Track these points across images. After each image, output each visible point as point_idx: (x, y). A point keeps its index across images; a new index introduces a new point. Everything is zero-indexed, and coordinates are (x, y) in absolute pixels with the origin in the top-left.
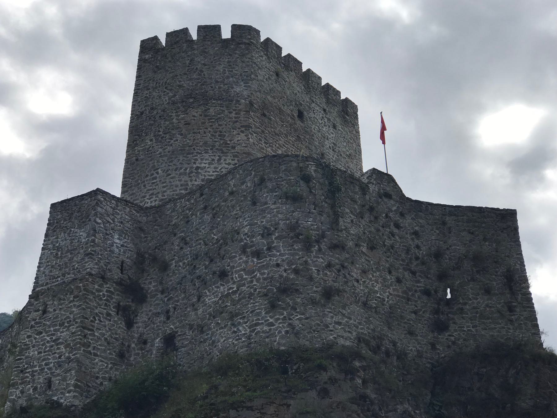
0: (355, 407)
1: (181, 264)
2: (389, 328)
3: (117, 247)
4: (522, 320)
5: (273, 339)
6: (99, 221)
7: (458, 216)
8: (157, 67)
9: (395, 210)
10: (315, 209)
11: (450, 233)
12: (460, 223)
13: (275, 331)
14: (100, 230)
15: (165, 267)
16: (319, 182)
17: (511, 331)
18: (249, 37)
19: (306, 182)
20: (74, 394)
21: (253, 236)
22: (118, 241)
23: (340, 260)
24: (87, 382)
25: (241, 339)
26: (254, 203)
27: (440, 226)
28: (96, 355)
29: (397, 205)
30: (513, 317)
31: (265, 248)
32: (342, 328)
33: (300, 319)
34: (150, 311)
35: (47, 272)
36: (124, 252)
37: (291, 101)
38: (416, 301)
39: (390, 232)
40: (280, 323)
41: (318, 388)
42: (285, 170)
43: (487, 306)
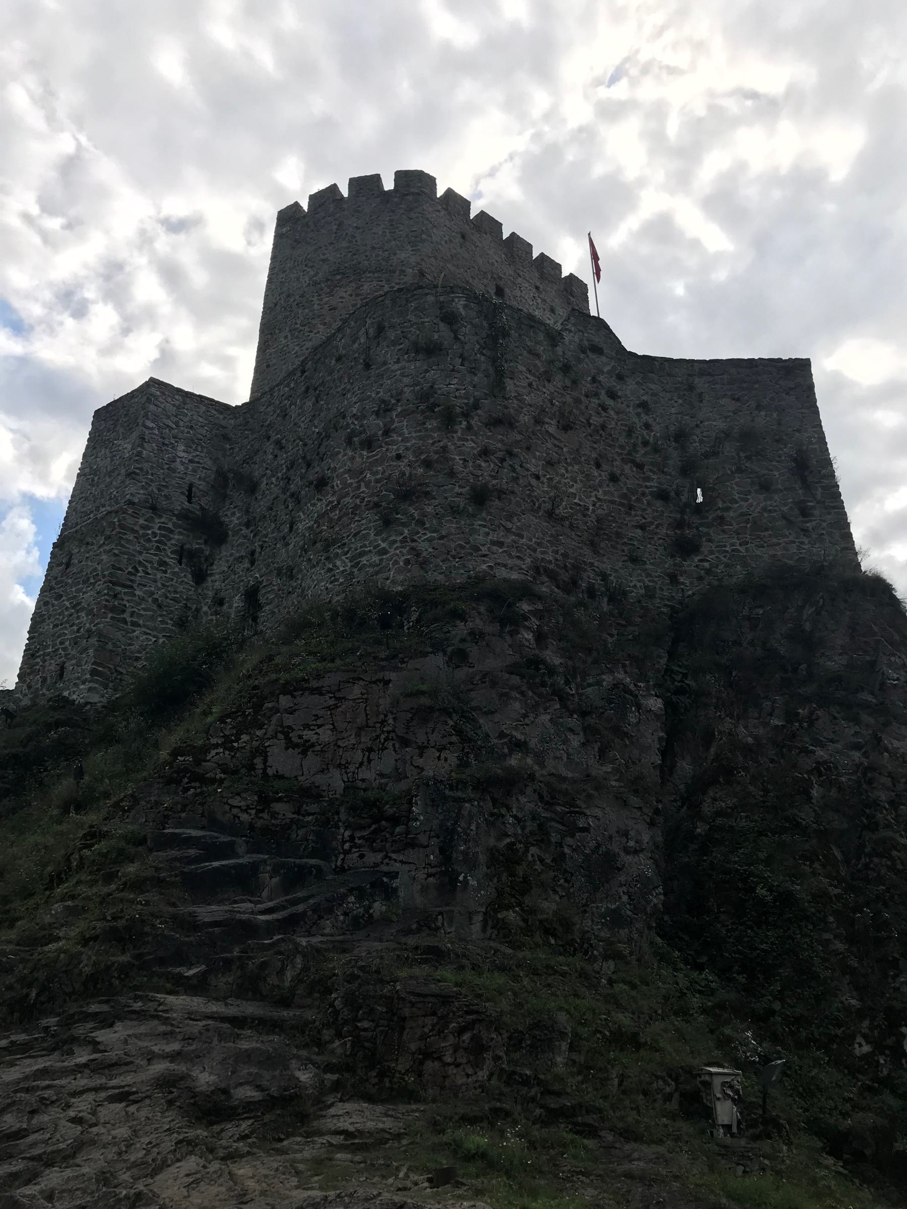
0: (516, 680)
1: (274, 480)
2: (596, 552)
3: (182, 463)
4: (823, 529)
5: (385, 575)
6: (151, 425)
7: (713, 376)
8: (296, 241)
9: (609, 372)
10: (462, 365)
11: (701, 401)
12: (718, 386)
13: (388, 562)
14: (151, 438)
15: (252, 488)
16: (471, 323)
17: (806, 547)
18: (419, 185)
19: (450, 324)
20: (91, 685)
21: (364, 417)
22: (182, 454)
23: (504, 444)
24: (115, 666)
25: (337, 580)
26: (367, 366)
27: (685, 392)
28: (135, 624)
29: (613, 364)
30: (808, 525)
31: (380, 433)
32: (502, 553)
33: (430, 540)
34: (231, 555)
35: (79, 507)
36: (194, 471)
37: (485, 273)
38: (644, 510)
39: (599, 405)
40: (396, 549)
41: (450, 649)
42: (416, 309)
43: (764, 509)
